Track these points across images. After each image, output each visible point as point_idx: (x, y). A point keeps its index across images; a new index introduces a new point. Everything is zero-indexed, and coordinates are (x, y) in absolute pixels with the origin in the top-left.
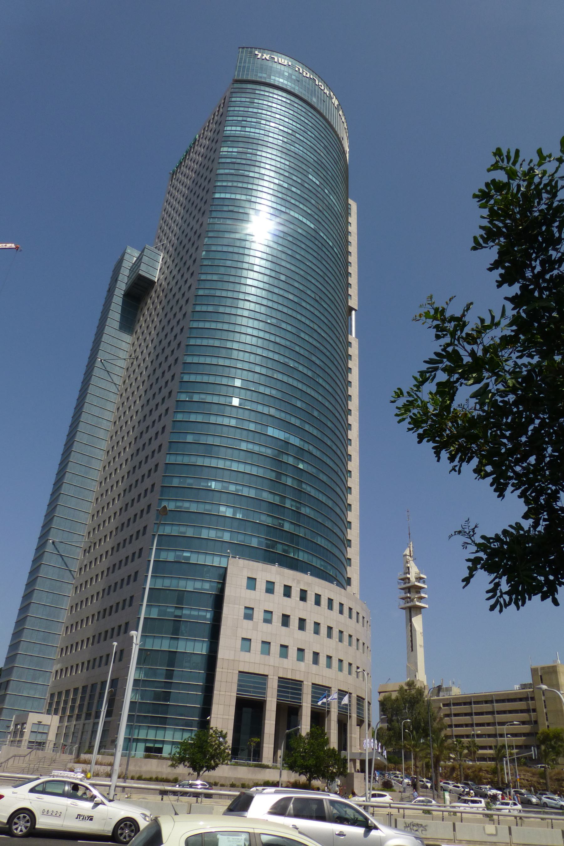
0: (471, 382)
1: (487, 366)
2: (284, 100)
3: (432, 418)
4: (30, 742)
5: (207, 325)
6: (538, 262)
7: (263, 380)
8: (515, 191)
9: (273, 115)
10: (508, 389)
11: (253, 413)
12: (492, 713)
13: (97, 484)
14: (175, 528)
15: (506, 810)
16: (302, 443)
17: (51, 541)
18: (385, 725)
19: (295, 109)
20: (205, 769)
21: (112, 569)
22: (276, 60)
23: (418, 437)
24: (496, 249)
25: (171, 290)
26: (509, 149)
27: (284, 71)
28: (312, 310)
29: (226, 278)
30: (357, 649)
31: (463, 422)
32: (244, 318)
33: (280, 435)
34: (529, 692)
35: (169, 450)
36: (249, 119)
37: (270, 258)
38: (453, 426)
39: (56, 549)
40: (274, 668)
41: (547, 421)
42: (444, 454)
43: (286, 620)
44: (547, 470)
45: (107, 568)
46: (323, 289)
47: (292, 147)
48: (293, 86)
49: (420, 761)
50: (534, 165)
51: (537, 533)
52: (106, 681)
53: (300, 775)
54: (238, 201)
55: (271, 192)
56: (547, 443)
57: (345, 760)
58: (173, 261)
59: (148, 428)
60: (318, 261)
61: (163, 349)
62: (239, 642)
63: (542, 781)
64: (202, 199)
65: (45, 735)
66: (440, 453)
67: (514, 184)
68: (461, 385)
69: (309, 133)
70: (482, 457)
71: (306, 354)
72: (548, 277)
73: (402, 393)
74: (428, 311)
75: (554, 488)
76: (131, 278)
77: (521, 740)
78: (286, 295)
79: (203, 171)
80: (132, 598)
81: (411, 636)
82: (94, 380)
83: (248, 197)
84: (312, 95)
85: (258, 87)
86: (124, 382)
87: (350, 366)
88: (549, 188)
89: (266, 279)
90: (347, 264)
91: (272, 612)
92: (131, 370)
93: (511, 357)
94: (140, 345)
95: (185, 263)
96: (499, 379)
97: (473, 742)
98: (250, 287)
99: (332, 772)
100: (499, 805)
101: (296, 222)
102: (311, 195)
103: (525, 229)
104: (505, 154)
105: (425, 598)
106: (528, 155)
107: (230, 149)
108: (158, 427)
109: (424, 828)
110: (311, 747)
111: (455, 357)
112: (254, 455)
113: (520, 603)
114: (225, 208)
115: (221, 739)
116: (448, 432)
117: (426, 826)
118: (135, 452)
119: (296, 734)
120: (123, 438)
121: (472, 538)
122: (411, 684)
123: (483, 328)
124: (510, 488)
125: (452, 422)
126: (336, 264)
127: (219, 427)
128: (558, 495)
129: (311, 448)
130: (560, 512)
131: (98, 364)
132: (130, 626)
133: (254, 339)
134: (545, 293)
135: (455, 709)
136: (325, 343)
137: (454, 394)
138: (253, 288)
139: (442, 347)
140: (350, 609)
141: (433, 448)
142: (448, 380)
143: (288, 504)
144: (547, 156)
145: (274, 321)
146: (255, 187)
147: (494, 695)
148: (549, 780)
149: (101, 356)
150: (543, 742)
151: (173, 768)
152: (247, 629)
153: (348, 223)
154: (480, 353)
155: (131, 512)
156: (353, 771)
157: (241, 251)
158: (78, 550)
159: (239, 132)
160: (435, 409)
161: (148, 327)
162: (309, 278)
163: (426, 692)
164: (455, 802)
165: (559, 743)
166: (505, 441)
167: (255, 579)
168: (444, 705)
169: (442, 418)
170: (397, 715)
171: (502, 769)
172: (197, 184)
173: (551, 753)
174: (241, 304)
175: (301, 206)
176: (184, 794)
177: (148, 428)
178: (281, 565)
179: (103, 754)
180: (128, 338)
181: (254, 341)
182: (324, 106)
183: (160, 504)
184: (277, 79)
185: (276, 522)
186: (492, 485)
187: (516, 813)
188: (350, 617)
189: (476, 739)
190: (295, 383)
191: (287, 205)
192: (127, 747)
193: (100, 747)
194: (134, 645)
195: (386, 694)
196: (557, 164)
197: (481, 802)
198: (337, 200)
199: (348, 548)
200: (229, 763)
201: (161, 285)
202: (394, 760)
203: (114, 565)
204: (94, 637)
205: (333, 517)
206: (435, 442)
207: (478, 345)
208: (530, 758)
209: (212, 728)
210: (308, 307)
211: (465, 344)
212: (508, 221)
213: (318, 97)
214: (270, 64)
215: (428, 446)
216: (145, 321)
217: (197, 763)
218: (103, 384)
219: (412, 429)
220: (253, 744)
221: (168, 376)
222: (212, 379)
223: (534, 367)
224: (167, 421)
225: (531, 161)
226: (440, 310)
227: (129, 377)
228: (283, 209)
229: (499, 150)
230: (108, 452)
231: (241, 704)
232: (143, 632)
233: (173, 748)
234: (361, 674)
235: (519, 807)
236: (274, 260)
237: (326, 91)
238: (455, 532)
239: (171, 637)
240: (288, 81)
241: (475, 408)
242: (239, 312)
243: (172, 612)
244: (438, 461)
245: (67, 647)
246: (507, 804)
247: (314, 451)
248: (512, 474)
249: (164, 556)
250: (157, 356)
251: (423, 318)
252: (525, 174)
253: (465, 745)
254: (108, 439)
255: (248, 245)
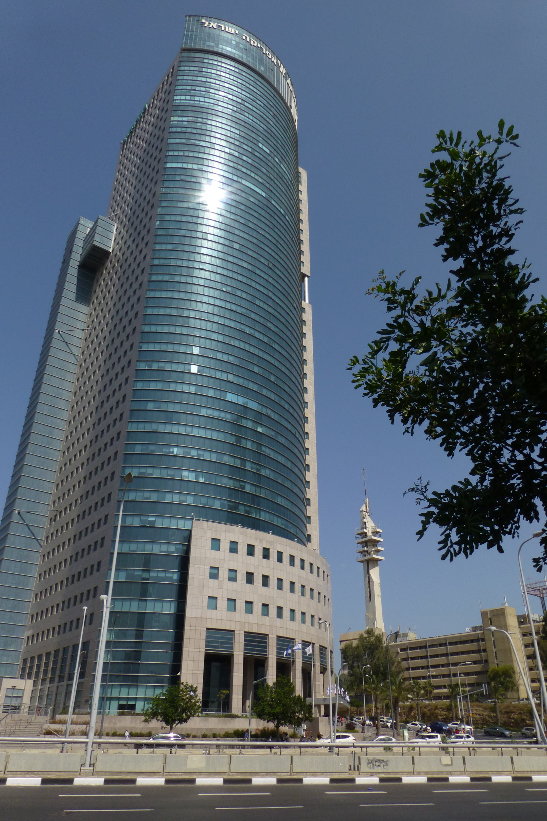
0: (421, 350)
1: (435, 336)
2: (232, 68)
3: (386, 384)
4: (5, 706)
5: (164, 294)
6: (480, 237)
7: (220, 347)
8: (458, 171)
9: (222, 84)
10: (454, 357)
11: (211, 380)
12: (446, 655)
13: (60, 454)
14: (139, 494)
15: (460, 742)
16: (260, 407)
17: (16, 512)
18: (347, 672)
19: (244, 78)
20: (177, 722)
21: (79, 536)
22: (223, 29)
23: (373, 402)
24: (441, 225)
25: (126, 260)
26: (451, 132)
27: (231, 40)
28: (266, 277)
29: (180, 248)
30: (319, 602)
31: (414, 386)
32: (200, 287)
33: (239, 400)
34: (480, 633)
35: (131, 418)
36: (198, 88)
37: (223, 227)
38: (406, 390)
39: (22, 519)
40: (240, 623)
41: (490, 384)
42: (398, 417)
43: (250, 578)
44: (491, 429)
45: (73, 535)
46: (277, 257)
47: (241, 116)
48: (241, 54)
49: (380, 703)
50: (475, 147)
51: (483, 487)
52: (78, 644)
53: (268, 722)
54: (190, 171)
55: (222, 161)
56: (490, 405)
57: (311, 706)
58: (127, 231)
59: (108, 397)
60: (270, 229)
61: (121, 319)
62: (206, 601)
63: (492, 714)
64: (153, 169)
65: (20, 699)
66: (394, 416)
67: (457, 164)
68: (411, 354)
69: (258, 102)
70: (432, 419)
71: (262, 321)
72: (489, 251)
73: (357, 361)
74: (380, 285)
75: (498, 446)
76: (85, 249)
77: (472, 679)
78: (240, 263)
79: (154, 141)
80: (99, 563)
81: (369, 587)
82: (52, 352)
83: (200, 166)
84: (259, 64)
85: (206, 56)
86: (83, 353)
87: (304, 331)
88: (488, 168)
89: (220, 247)
90: (299, 231)
91: (236, 571)
92: (89, 340)
93: (457, 327)
94: (97, 316)
95: (139, 233)
96: (447, 348)
97: (429, 682)
98: (205, 256)
99: (299, 718)
100: (454, 738)
101: (248, 191)
102: (262, 164)
103: (468, 207)
104: (448, 136)
105: (381, 550)
106: (470, 137)
107: (180, 119)
108: (119, 396)
109: (385, 763)
110: (277, 696)
111: (406, 328)
112: (214, 420)
113: (469, 552)
114: (178, 178)
115: (192, 693)
116: (401, 396)
117: (387, 761)
118: (97, 421)
119: (263, 685)
120: (84, 408)
121: (425, 494)
122: (370, 632)
123: (431, 301)
124: (459, 447)
125: (404, 388)
126: (288, 231)
127: (179, 394)
128: (502, 452)
129: (269, 412)
130: (503, 468)
131: (56, 335)
132: (99, 590)
133: (210, 307)
134: (487, 266)
135: (411, 653)
136: (279, 310)
137: (406, 361)
138: (208, 257)
139: (394, 319)
140: (311, 564)
141: (388, 411)
142: (400, 349)
143: (248, 466)
144: (487, 137)
145: (229, 289)
146: (206, 156)
147: (448, 638)
148: (498, 713)
149: (58, 327)
150: (493, 679)
151: (147, 723)
152: (213, 587)
153: (298, 191)
154: (428, 324)
155: (95, 480)
156: (318, 716)
157: (195, 220)
158: (44, 519)
159: (189, 101)
160: (389, 375)
161: (104, 298)
162: (262, 246)
163: (384, 639)
164: (413, 738)
165: (508, 679)
166: (452, 404)
167: (220, 540)
168: (401, 650)
169: (395, 383)
170: (357, 661)
171: (456, 706)
172: (148, 154)
173: (501, 688)
174: (196, 273)
175: (252, 175)
176: (158, 746)
177: (108, 397)
178: (244, 525)
179: (78, 714)
180: (85, 309)
181: (210, 309)
182: (272, 75)
183: (123, 472)
184: (225, 47)
185: (237, 484)
186: (442, 445)
187: (469, 745)
188: (311, 572)
189: (432, 680)
190: (252, 349)
191: (239, 173)
192: (101, 706)
193: (75, 708)
194: (105, 608)
195: (348, 642)
196: (495, 145)
197: (437, 737)
198: (287, 168)
199: (308, 507)
200: (200, 715)
201: (116, 256)
202: (356, 702)
203: (81, 532)
204: (64, 602)
205: (293, 478)
206: (389, 405)
207: (427, 316)
208: (482, 694)
209: (182, 683)
210: (262, 274)
211: (415, 315)
212: (452, 199)
213: (266, 65)
214: (217, 32)
215: (383, 410)
216: (102, 292)
217: (169, 717)
218: (61, 355)
219: (367, 394)
220: (222, 696)
221: (127, 345)
222: (170, 348)
223: (479, 333)
224: (127, 390)
225: (472, 142)
226: (391, 284)
227: (88, 347)
228: (235, 178)
229: (442, 132)
230: (70, 422)
231: (210, 659)
232: (113, 595)
233: (146, 704)
234: (323, 625)
235: (472, 739)
236: (227, 229)
237: (273, 60)
238: (409, 490)
239: (140, 599)
240: (236, 50)
241: (425, 374)
242: (195, 281)
243: (139, 575)
244: (392, 423)
245: (37, 614)
246: (461, 737)
247: (273, 415)
248: (459, 434)
249: (129, 521)
250: (115, 326)
251: (376, 292)
252: (467, 156)
253: (421, 686)
254: (69, 409)
255: (201, 214)
